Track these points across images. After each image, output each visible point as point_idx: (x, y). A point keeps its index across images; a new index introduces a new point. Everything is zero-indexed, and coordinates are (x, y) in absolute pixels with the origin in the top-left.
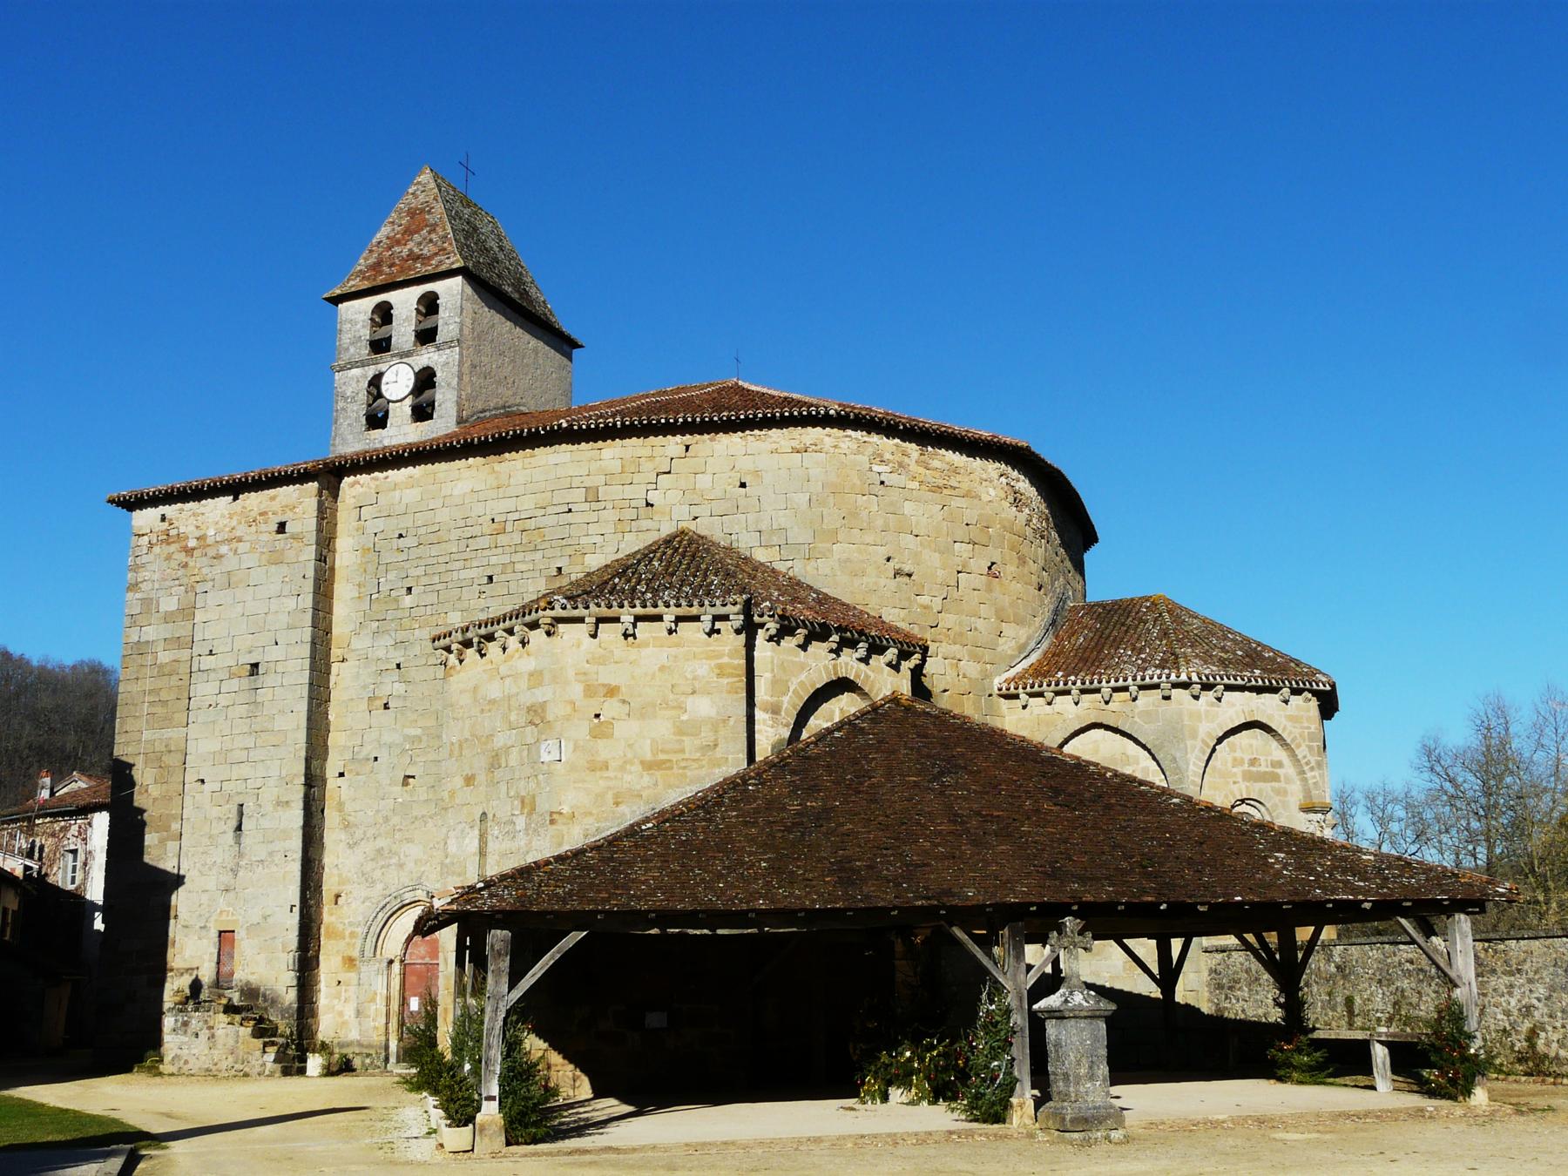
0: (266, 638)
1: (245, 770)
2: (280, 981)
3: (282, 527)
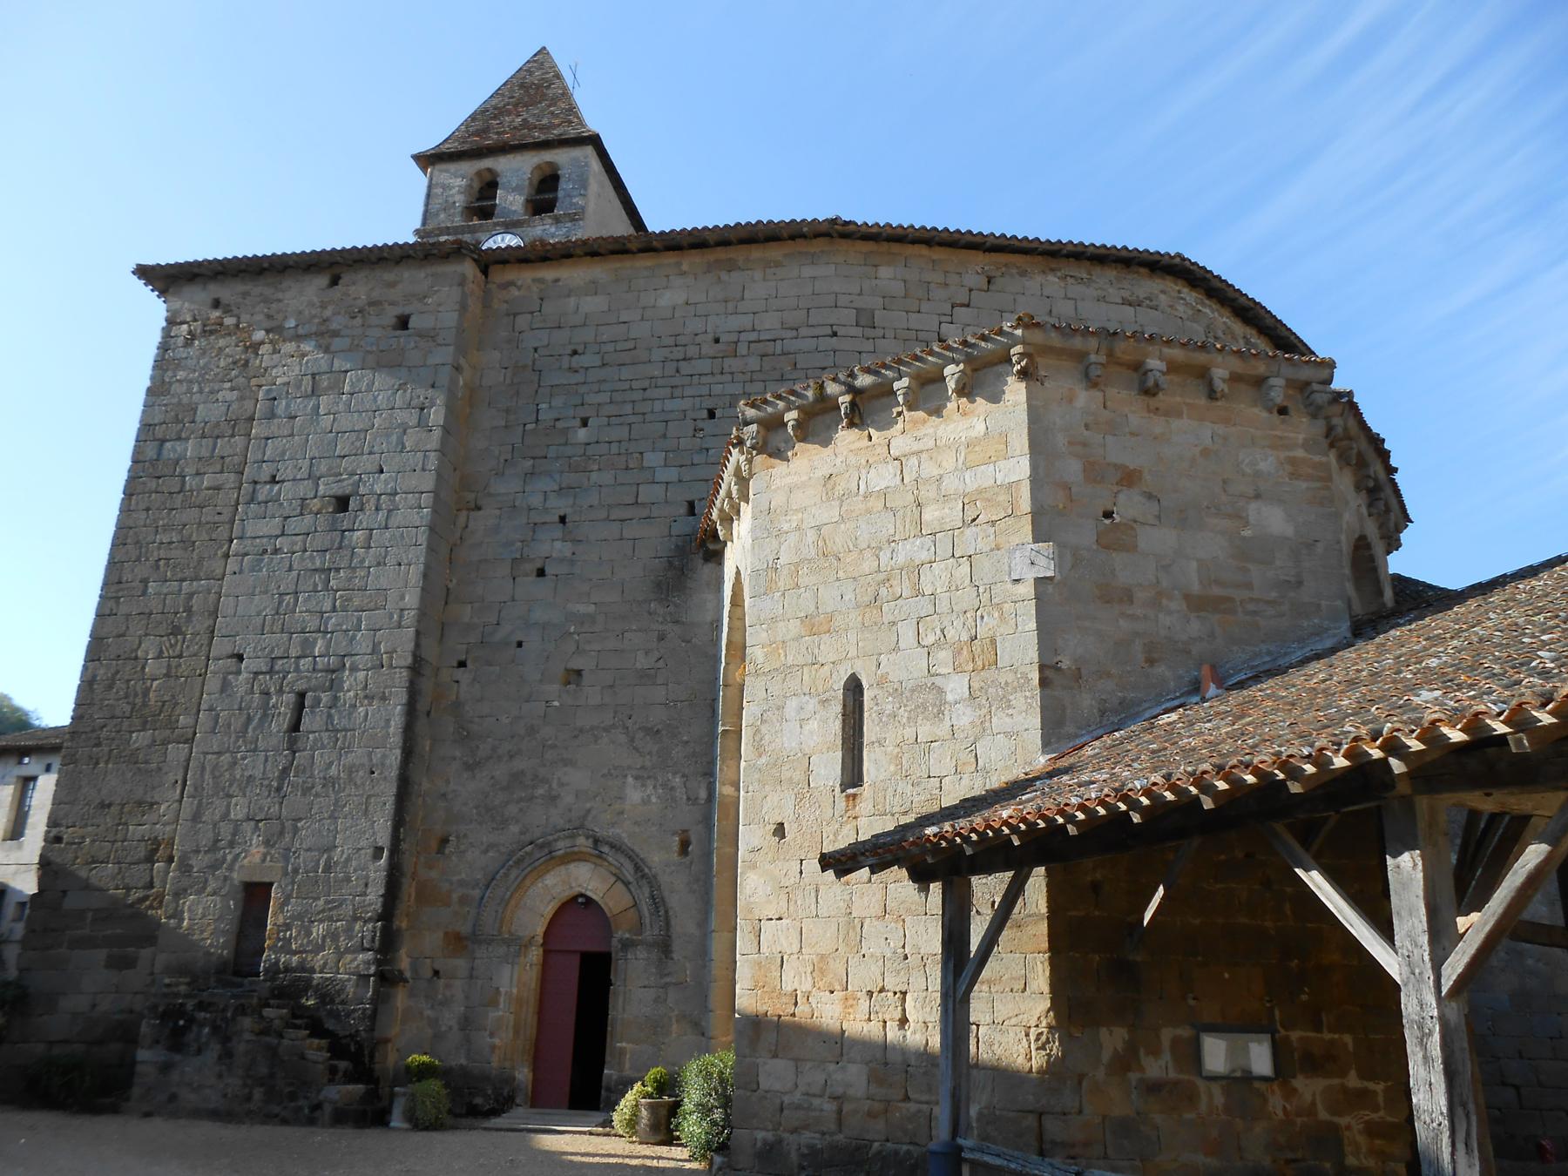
0: (367, 463)
3: (403, 323)
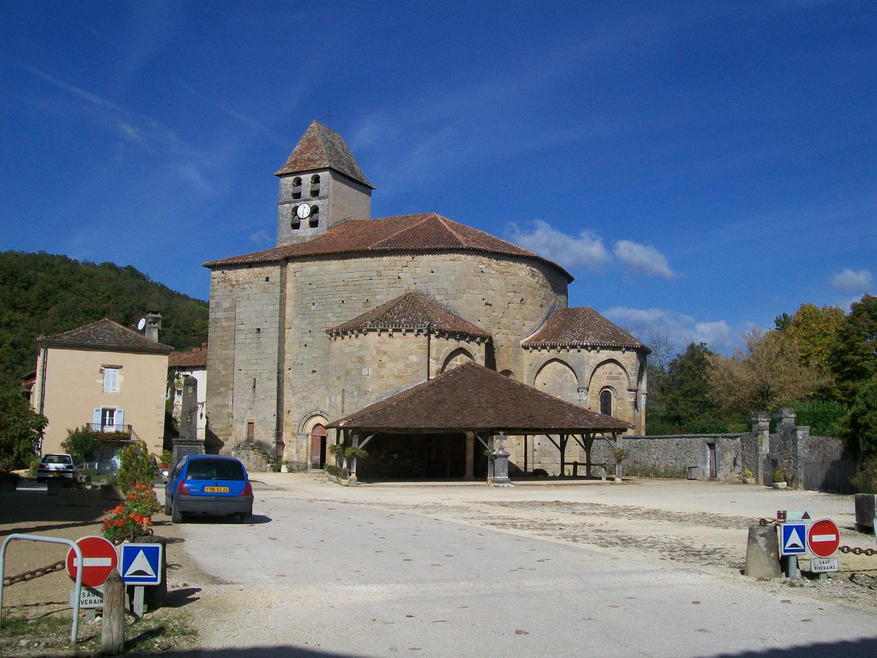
1: (256, 367)
2: (271, 440)
3: (267, 279)
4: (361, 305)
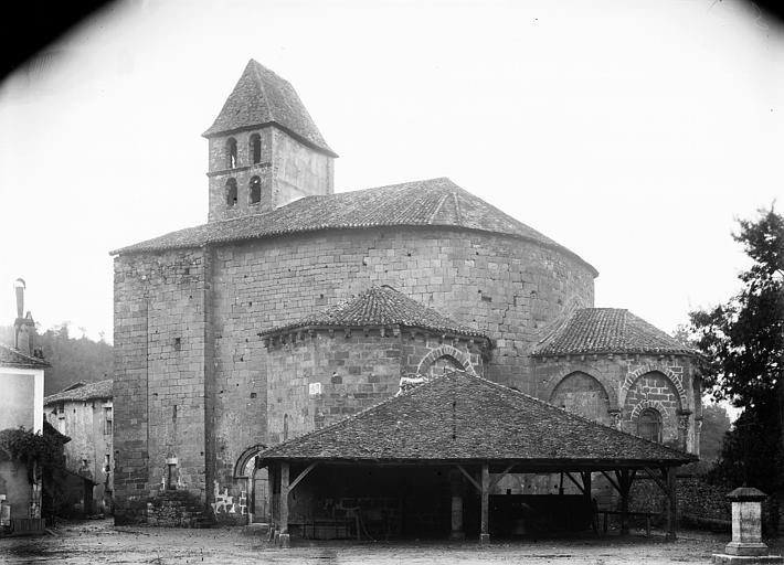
4: (313, 303)
